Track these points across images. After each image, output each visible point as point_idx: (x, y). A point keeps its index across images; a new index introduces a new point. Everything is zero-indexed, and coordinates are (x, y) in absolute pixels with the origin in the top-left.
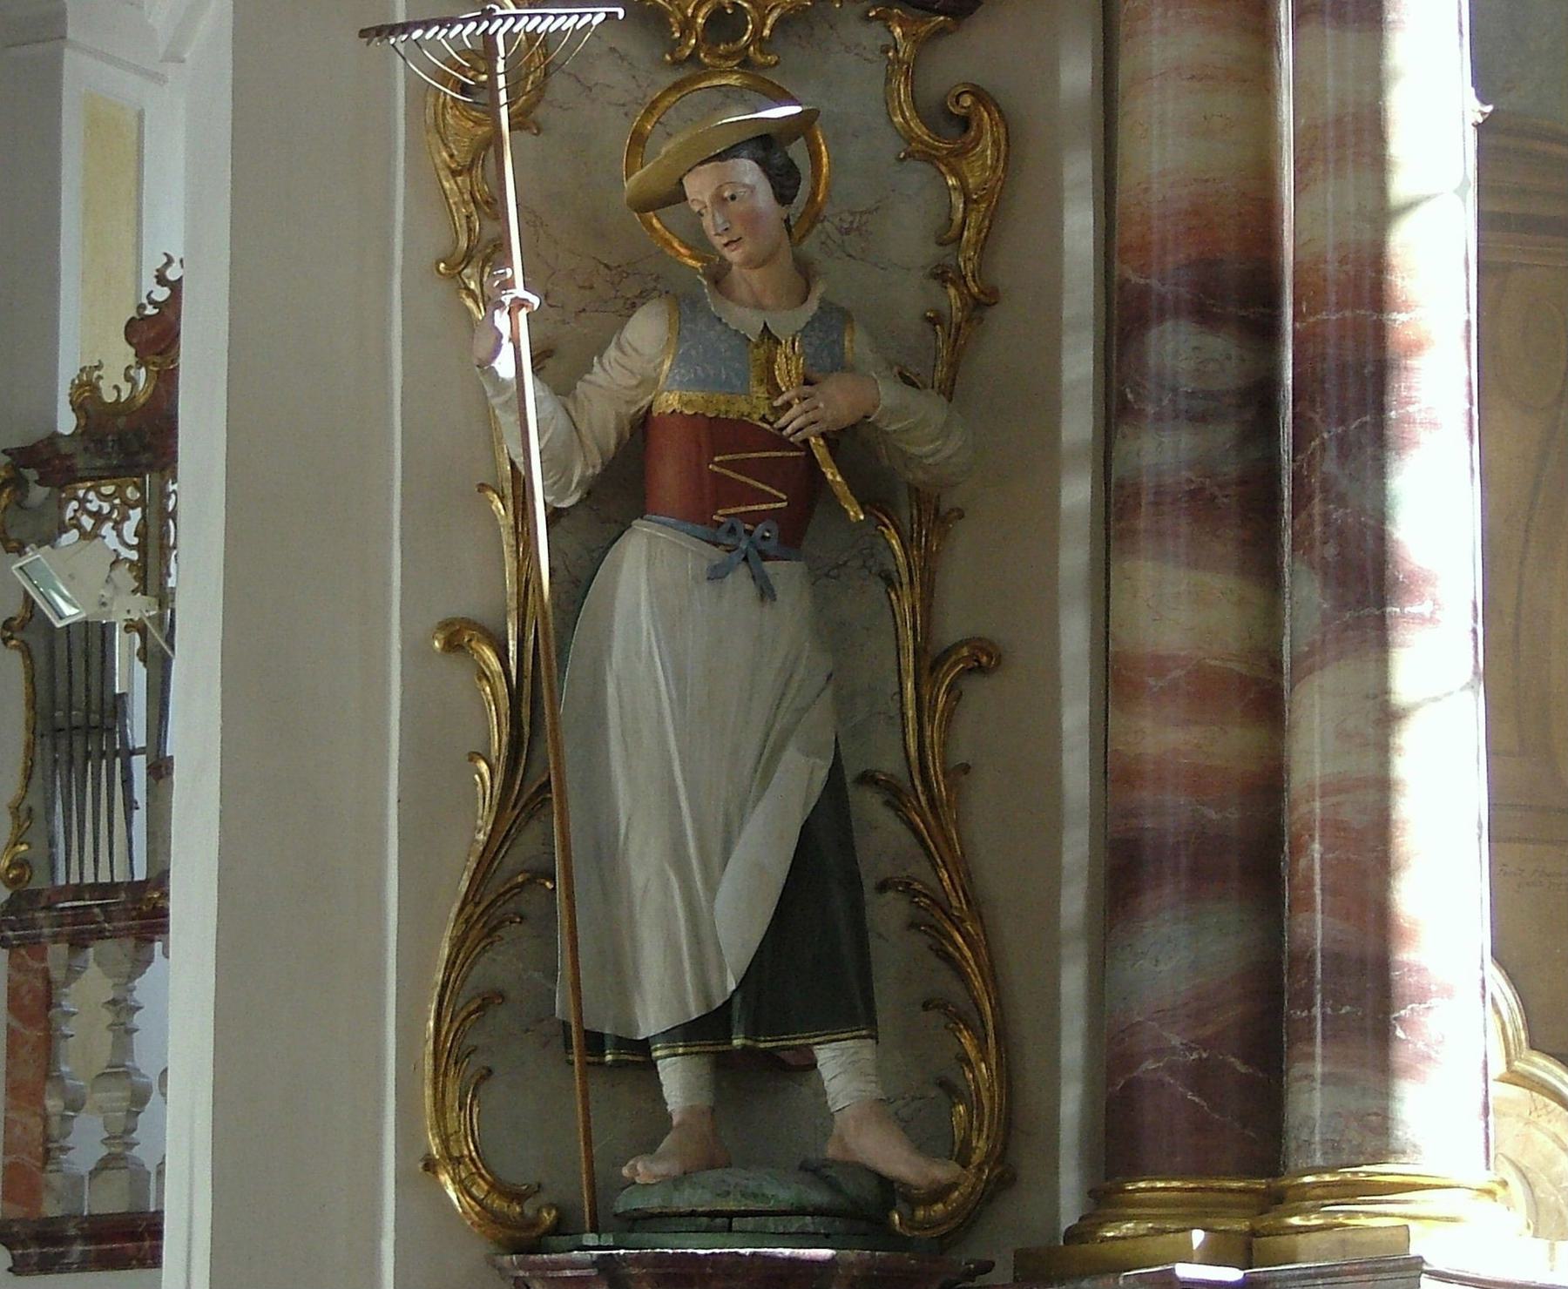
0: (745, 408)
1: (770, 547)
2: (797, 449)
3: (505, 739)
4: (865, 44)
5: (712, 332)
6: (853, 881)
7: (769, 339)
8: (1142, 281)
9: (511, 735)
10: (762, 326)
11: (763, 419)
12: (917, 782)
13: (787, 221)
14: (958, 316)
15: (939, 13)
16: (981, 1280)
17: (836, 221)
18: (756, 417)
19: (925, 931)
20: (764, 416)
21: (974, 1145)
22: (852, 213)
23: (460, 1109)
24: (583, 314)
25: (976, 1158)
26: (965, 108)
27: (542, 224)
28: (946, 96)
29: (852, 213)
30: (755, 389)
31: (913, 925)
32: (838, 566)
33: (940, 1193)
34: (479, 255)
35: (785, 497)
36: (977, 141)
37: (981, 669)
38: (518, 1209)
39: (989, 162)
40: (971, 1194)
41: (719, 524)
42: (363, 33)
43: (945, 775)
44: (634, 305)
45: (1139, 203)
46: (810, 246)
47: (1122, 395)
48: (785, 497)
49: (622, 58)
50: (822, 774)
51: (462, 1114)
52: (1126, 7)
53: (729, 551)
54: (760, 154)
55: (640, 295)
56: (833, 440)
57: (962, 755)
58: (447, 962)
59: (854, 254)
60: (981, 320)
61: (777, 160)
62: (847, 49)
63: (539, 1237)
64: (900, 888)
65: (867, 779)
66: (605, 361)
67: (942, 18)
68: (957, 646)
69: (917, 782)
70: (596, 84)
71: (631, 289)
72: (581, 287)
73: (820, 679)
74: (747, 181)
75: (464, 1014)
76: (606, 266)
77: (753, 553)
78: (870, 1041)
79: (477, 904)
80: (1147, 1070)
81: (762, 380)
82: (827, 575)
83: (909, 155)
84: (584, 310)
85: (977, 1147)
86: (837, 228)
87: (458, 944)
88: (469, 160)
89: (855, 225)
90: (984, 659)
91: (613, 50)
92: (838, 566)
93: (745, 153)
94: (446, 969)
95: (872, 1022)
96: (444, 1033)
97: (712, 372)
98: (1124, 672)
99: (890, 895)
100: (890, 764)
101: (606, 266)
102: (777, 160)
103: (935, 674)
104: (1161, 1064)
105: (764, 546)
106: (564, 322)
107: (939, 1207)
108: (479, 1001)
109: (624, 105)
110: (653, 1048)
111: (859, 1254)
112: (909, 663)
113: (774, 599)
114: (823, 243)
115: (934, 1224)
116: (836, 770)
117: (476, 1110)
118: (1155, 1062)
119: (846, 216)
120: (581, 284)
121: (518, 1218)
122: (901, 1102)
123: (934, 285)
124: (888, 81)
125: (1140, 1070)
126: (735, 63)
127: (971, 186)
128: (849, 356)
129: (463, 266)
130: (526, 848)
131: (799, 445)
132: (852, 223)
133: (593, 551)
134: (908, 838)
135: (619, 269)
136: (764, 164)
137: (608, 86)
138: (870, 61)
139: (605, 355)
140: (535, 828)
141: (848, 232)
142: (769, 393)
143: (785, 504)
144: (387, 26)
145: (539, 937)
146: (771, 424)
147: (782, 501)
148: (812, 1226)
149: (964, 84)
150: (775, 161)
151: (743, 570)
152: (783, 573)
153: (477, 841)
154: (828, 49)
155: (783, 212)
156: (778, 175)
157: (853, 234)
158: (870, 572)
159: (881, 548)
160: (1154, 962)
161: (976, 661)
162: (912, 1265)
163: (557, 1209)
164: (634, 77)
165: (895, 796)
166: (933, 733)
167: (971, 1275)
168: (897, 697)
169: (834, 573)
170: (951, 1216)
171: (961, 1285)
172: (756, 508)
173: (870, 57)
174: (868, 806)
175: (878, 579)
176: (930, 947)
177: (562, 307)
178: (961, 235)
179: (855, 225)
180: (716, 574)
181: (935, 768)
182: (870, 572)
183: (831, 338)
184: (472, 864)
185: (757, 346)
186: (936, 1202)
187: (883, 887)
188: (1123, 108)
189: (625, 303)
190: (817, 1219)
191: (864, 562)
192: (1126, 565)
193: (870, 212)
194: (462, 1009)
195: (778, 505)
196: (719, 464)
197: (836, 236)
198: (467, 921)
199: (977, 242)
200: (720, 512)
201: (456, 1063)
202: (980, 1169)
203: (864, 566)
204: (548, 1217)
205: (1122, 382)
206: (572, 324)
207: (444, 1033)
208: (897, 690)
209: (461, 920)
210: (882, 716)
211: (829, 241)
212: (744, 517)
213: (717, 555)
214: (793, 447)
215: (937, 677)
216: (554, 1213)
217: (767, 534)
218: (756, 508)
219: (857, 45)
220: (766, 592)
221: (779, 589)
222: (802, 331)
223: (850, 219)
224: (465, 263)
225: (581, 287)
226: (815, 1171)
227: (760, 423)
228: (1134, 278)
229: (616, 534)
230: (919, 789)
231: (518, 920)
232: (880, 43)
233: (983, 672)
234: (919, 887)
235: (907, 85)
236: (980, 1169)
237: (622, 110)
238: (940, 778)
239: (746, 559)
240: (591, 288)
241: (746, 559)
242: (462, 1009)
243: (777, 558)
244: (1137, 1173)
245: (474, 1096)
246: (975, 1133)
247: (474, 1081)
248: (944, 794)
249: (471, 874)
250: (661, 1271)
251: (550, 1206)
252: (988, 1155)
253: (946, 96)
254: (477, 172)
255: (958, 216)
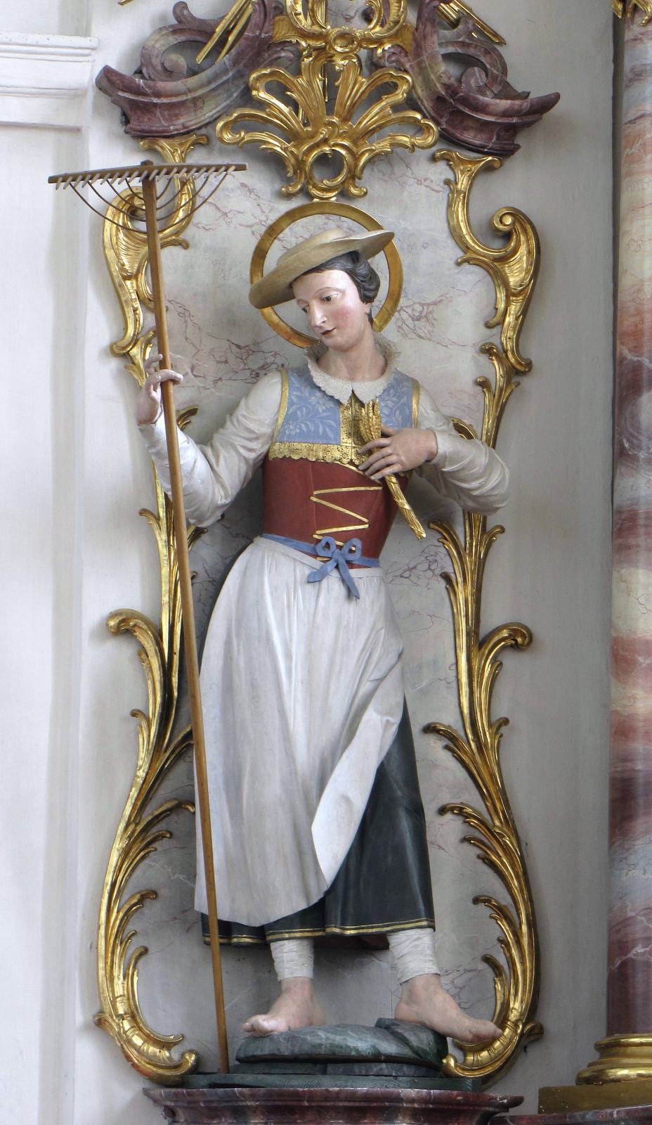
0: (337, 455)
1: (356, 557)
2: (379, 485)
3: (159, 699)
4: (433, 178)
5: (313, 398)
6: (417, 811)
7: (355, 402)
8: (636, 359)
9: (163, 697)
10: (351, 392)
11: (351, 463)
12: (469, 731)
13: (370, 315)
14: (501, 381)
15: (488, 154)
16: (513, 1111)
17: (409, 310)
18: (345, 461)
19: (474, 844)
20: (351, 460)
21: (511, 1005)
22: (422, 305)
23: (124, 978)
24: (219, 383)
25: (513, 1016)
26: (508, 225)
27: (189, 315)
28: (493, 217)
29: (422, 305)
30: (345, 441)
31: (466, 840)
32: (410, 570)
33: (484, 1042)
34: (142, 338)
35: (365, 520)
36: (515, 251)
37: (516, 647)
38: (167, 1054)
39: (525, 265)
40: (509, 1044)
41: (319, 541)
42: (52, 180)
43: (490, 725)
44: (257, 375)
45: (633, 300)
46: (390, 332)
47: (622, 445)
48: (365, 520)
49: (251, 191)
50: (394, 729)
51: (126, 982)
52: (626, 153)
53: (325, 562)
54: (350, 266)
55: (262, 368)
56: (403, 478)
57: (501, 711)
58: (115, 868)
59: (423, 335)
60: (518, 384)
61: (362, 270)
62: (419, 182)
63: (182, 1076)
64: (455, 812)
65: (430, 729)
66: (235, 420)
67: (490, 158)
68: (498, 630)
69: (469, 731)
70: (230, 211)
71: (255, 362)
72: (218, 362)
73: (392, 657)
74: (339, 286)
75: (127, 907)
76: (238, 347)
77: (342, 561)
78: (429, 930)
79: (137, 825)
80: (637, 953)
81: (350, 434)
82: (401, 576)
83: (467, 261)
84: (221, 379)
85: (513, 1008)
86: (410, 316)
87: (125, 853)
88: (136, 266)
89: (424, 313)
90: (519, 640)
91: (243, 185)
92: (410, 570)
93: (338, 265)
94: (114, 872)
95: (430, 914)
96: (111, 925)
97: (312, 429)
98: (621, 652)
99: (449, 816)
100: (449, 718)
101: (238, 347)
102: (362, 270)
103: (482, 650)
104: (648, 949)
105: (350, 557)
106: (205, 388)
107: (485, 1054)
108: (138, 896)
109: (251, 226)
110: (267, 933)
111: (418, 1092)
112: (463, 641)
113: (358, 597)
114: (400, 327)
115: (482, 1066)
116: (405, 725)
117: (136, 979)
118: (643, 947)
119: (420, 308)
120: (218, 359)
121: (167, 1060)
122: (456, 974)
123: (483, 358)
124: (449, 206)
125: (632, 953)
126: (334, 194)
127: (511, 284)
128: (415, 413)
129: (131, 347)
130: (167, 790)
131: (378, 482)
132: (421, 312)
133: (226, 559)
134: (462, 774)
135: (247, 348)
136: (352, 274)
137: (239, 212)
138: (438, 192)
139: (234, 414)
140: (181, 767)
141: (418, 319)
142: (355, 443)
143: (367, 526)
144: (70, 175)
145: (183, 848)
146: (357, 466)
147: (363, 523)
148: (386, 1070)
149: (508, 208)
150: (359, 271)
151: (335, 574)
152: (362, 577)
153: (138, 777)
154: (404, 183)
155: (366, 308)
156: (362, 281)
157: (423, 320)
158: (434, 573)
159: (442, 556)
160: (643, 871)
161: (512, 640)
162: (459, 1100)
163: (197, 1054)
164: (259, 205)
165: (452, 742)
166: (481, 695)
167: (505, 1108)
168: (454, 667)
169: (406, 574)
170: (492, 1061)
171: (498, 1115)
172: (345, 529)
173: (436, 188)
174: (431, 751)
175: (440, 579)
176: (479, 857)
177: (204, 377)
178: (504, 320)
179: (424, 313)
180: (315, 579)
181: (482, 721)
182: (434, 573)
183: (402, 401)
184: (134, 793)
185: (347, 408)
186: (483, 1050)
187: (442, 811)
188: (624, 227)
189: (251, 374)
190: (390, 1065)
191: (430, 566)
192: (623, 571)
193: (435, 303)
194: (125, 903)
195: (361, 527)
196: (317, 496)
197: (410, 322)
198: (130, 837)
199: (515, 325)
200: (318, 532)
201: (121, 943)
202: (516, 1025)
203: (429, 569)
204: (191, 1059)
205: (620, 435)
206: (212, 390)
207: (111, 925)
208: (454, 661)
209: (126, 836)
210: (443, 682)
211: (404, 326)
212: (335, 535)
213: (317, 563)
214: (372, 483)
215: (484, 653)
216: (193, 1057)
217: (354, 549)
218: (345, 529)
219: (425, 180)
220: (351, 593)
221: (362, 593)
222: (380, 396)
223: (420, 308)
224: (132, 344)
225: (218, 362)
226: (387, 1028)
227: (347, 466)
228: (630, 356)
229: (240, 547)
230: (470, 736)
231: (168, 836)
232: (443, 177)
233: (518, 647)
234: (469, 810)
235: (464, 208)
236: (516, 1025)
237: (249, 230)
238: (486, 729)
239: (337, 567)
240: (226, 362)
241: (337, 567)
242: (125, 903)
243: (360, 566)
244: (633, 1031)
245: (134, 968)
246: (512, 998)
247: (134, 957)
248: (489, 740)
249: (133, 801)
250: (270, 1104)
251: (191, 1052)
252: (522, 1014)
253: (494, 215)
254: (142, 278)
255: (502, 306)
